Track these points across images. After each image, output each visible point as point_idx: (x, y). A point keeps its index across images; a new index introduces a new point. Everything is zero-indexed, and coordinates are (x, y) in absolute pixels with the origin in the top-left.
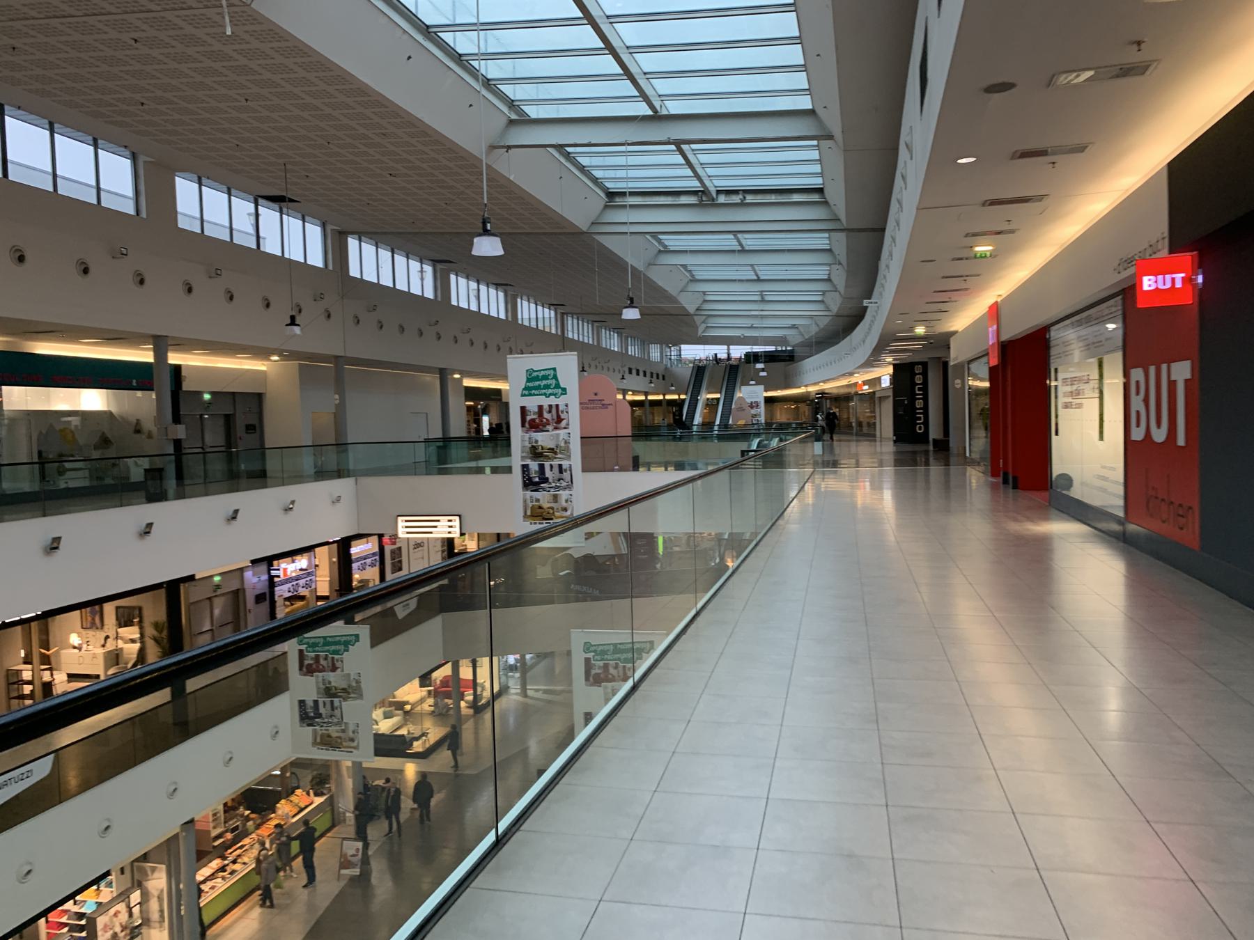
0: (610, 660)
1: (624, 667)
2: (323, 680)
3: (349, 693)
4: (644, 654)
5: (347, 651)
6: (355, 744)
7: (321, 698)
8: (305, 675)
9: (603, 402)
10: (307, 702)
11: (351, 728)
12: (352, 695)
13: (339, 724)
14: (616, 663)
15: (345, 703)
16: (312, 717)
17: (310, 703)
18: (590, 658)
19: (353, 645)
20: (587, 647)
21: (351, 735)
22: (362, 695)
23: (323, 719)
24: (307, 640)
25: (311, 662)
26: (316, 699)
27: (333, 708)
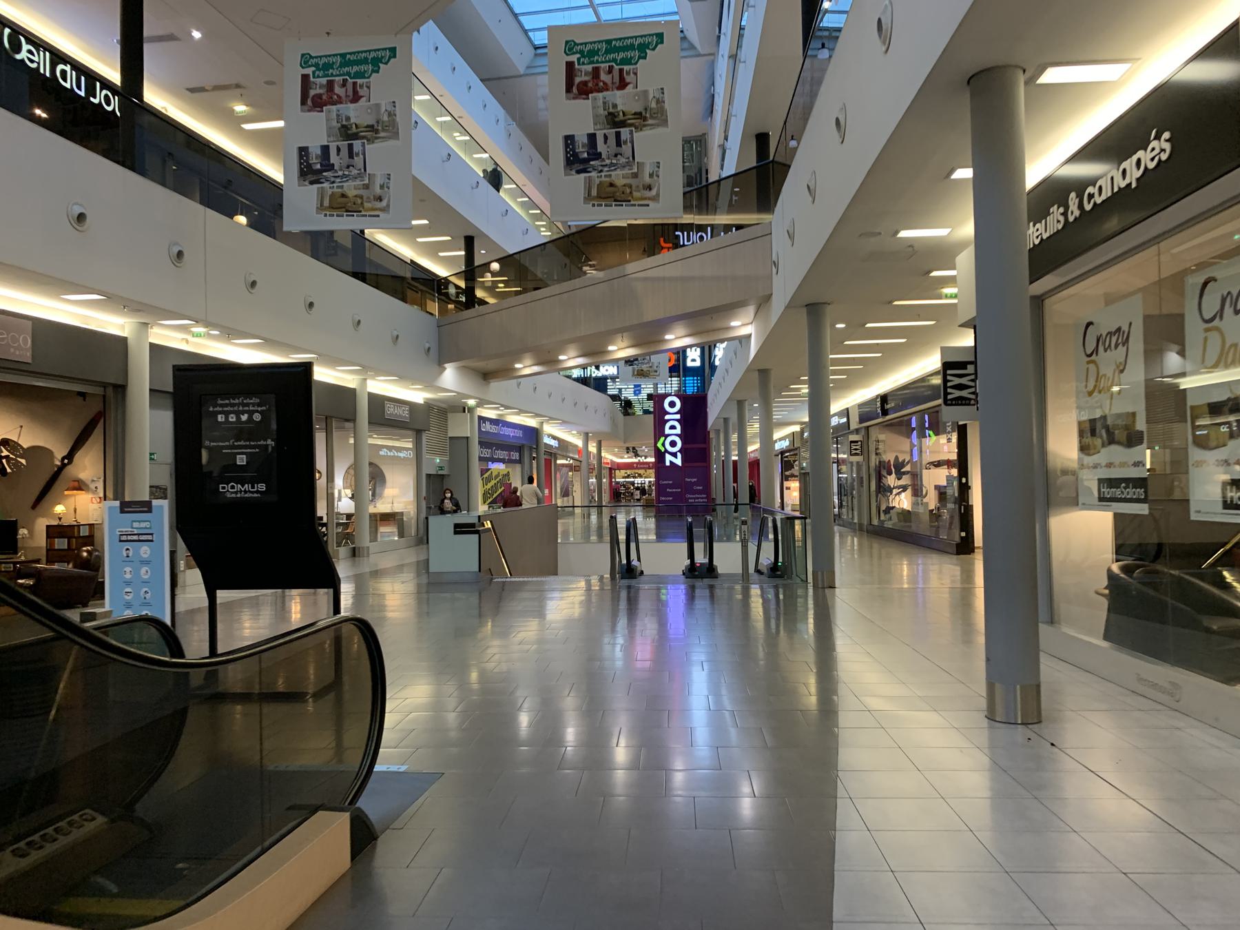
0: (602, 62)
3: (377, 132)
4: (381, 65)
5: (645, 58)
7: (332, 142)
8: (309, 111)
11: (647, 170)
12: (382, 134)
13: (628, 164)
14: (343, 80)
15: (369, 146)
16: (318, 170)
17: (581, 139)
18: (308, 76)
19: (386, 63)
20: (306, 60)
23: (603, 160)
24: (314, 61)
26: (592, 131)
27: (351, 155)
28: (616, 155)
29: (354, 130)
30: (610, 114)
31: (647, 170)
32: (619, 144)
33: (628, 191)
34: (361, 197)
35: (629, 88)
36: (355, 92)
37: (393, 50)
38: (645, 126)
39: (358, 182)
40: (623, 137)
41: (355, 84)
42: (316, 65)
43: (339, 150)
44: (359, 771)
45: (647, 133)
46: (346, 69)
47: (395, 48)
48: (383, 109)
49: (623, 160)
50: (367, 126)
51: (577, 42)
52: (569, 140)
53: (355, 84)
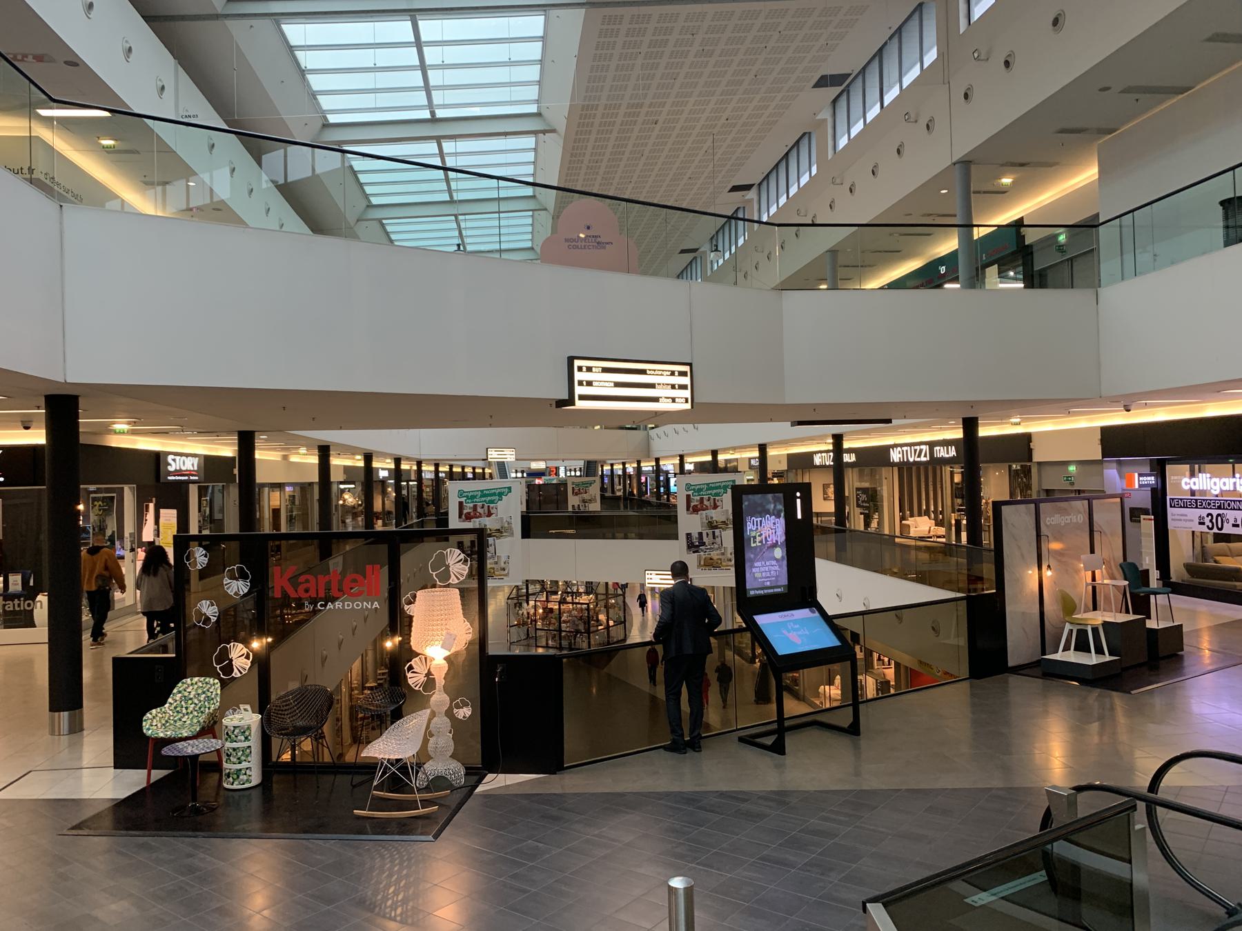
1: (489, 506)
2: (706, 516)
3: (502, 533)
5: (501, 500)
6: (506, 572)
8: (463, 521)
9: (599, 239)
10: (465, 543)
11: (503, 560)
12: (504, 534)
17: (695, 535)
20: (461, 494)
21: (503, 565)
22: (513, 534)
24: (693, 487)
25: (470, 511)
26: (700, 531)
28: (713, 543)
29: (715, 524)
30: (709, 522)
31: (503, 560)
32: (714, 538)
33: (492, 571)
34: (721, 559)
35: (719, 509)
36: (715, 504)
37: (510, 488)
38: (502, 536)
39: (718, 552)
40: (716, 534)
41: (714, 499)
42: (694, 490)
43: (707, 534)
44: (1096, 822)
45: (502, 540)
46: (710, 492)
47: (511, 487)
48: (505, 521)
49: (716, 546)
50: (496, 530)
51: (465, 491)
52: (689, 536)
53: (714, 499)
